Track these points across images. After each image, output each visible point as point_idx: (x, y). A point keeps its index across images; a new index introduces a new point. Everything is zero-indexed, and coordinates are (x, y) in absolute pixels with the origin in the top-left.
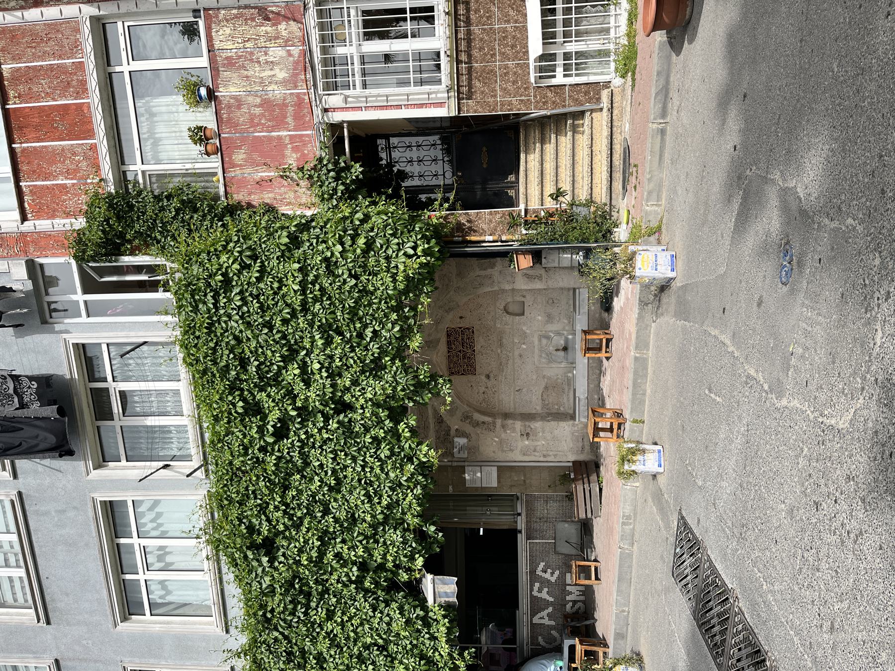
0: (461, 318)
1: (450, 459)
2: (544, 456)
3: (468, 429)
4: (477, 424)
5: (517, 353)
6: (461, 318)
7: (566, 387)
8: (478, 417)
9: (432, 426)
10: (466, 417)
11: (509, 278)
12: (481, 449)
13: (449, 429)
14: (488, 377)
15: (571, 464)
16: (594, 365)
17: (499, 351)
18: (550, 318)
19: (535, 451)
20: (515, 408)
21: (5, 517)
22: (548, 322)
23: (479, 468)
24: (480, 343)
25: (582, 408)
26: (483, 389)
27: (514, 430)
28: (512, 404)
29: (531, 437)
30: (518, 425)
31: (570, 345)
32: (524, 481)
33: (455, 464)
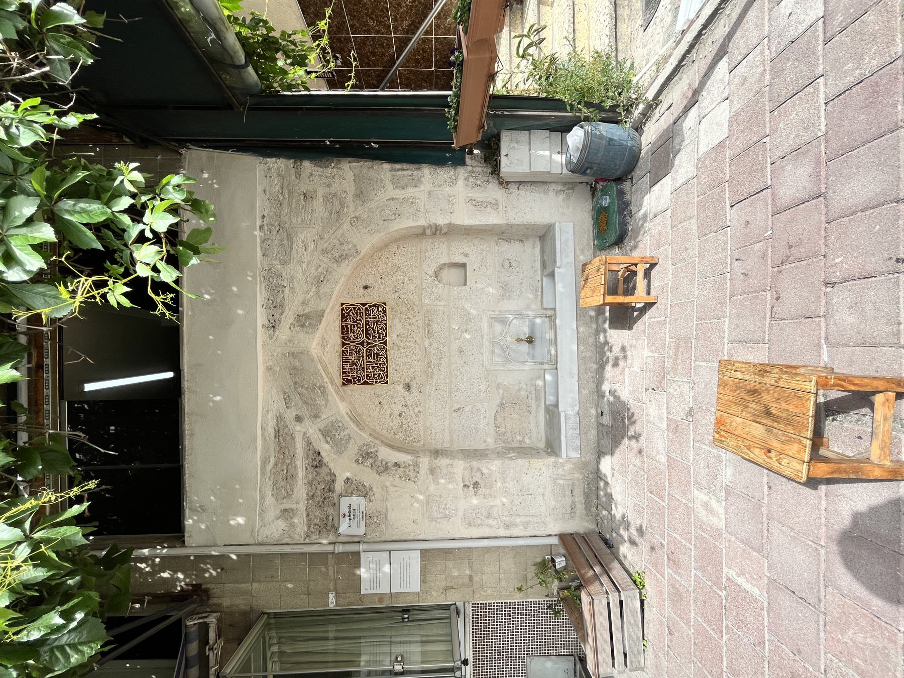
0: (366, 287)
1: (332, 538)
2: (507, 526)
3: (367, 476)
4: (384, 468)
5: (455, 346)
6: (366, 287)
7: (533, 404)
8: (386, 454)
9: (301, 473)
12: (392, 516)
14: (408, 387)
15: (555, 541)
16: (588, 354)
17: (427, 343)
18: (506, 291)
22: (502, 297)
23: (386, 555)
26: (398, 408)
27: (451, 478)
29: (482, 490)
30: (460, 467)
31: (537, 335)
32: (471, 577)
33: (340, 549)
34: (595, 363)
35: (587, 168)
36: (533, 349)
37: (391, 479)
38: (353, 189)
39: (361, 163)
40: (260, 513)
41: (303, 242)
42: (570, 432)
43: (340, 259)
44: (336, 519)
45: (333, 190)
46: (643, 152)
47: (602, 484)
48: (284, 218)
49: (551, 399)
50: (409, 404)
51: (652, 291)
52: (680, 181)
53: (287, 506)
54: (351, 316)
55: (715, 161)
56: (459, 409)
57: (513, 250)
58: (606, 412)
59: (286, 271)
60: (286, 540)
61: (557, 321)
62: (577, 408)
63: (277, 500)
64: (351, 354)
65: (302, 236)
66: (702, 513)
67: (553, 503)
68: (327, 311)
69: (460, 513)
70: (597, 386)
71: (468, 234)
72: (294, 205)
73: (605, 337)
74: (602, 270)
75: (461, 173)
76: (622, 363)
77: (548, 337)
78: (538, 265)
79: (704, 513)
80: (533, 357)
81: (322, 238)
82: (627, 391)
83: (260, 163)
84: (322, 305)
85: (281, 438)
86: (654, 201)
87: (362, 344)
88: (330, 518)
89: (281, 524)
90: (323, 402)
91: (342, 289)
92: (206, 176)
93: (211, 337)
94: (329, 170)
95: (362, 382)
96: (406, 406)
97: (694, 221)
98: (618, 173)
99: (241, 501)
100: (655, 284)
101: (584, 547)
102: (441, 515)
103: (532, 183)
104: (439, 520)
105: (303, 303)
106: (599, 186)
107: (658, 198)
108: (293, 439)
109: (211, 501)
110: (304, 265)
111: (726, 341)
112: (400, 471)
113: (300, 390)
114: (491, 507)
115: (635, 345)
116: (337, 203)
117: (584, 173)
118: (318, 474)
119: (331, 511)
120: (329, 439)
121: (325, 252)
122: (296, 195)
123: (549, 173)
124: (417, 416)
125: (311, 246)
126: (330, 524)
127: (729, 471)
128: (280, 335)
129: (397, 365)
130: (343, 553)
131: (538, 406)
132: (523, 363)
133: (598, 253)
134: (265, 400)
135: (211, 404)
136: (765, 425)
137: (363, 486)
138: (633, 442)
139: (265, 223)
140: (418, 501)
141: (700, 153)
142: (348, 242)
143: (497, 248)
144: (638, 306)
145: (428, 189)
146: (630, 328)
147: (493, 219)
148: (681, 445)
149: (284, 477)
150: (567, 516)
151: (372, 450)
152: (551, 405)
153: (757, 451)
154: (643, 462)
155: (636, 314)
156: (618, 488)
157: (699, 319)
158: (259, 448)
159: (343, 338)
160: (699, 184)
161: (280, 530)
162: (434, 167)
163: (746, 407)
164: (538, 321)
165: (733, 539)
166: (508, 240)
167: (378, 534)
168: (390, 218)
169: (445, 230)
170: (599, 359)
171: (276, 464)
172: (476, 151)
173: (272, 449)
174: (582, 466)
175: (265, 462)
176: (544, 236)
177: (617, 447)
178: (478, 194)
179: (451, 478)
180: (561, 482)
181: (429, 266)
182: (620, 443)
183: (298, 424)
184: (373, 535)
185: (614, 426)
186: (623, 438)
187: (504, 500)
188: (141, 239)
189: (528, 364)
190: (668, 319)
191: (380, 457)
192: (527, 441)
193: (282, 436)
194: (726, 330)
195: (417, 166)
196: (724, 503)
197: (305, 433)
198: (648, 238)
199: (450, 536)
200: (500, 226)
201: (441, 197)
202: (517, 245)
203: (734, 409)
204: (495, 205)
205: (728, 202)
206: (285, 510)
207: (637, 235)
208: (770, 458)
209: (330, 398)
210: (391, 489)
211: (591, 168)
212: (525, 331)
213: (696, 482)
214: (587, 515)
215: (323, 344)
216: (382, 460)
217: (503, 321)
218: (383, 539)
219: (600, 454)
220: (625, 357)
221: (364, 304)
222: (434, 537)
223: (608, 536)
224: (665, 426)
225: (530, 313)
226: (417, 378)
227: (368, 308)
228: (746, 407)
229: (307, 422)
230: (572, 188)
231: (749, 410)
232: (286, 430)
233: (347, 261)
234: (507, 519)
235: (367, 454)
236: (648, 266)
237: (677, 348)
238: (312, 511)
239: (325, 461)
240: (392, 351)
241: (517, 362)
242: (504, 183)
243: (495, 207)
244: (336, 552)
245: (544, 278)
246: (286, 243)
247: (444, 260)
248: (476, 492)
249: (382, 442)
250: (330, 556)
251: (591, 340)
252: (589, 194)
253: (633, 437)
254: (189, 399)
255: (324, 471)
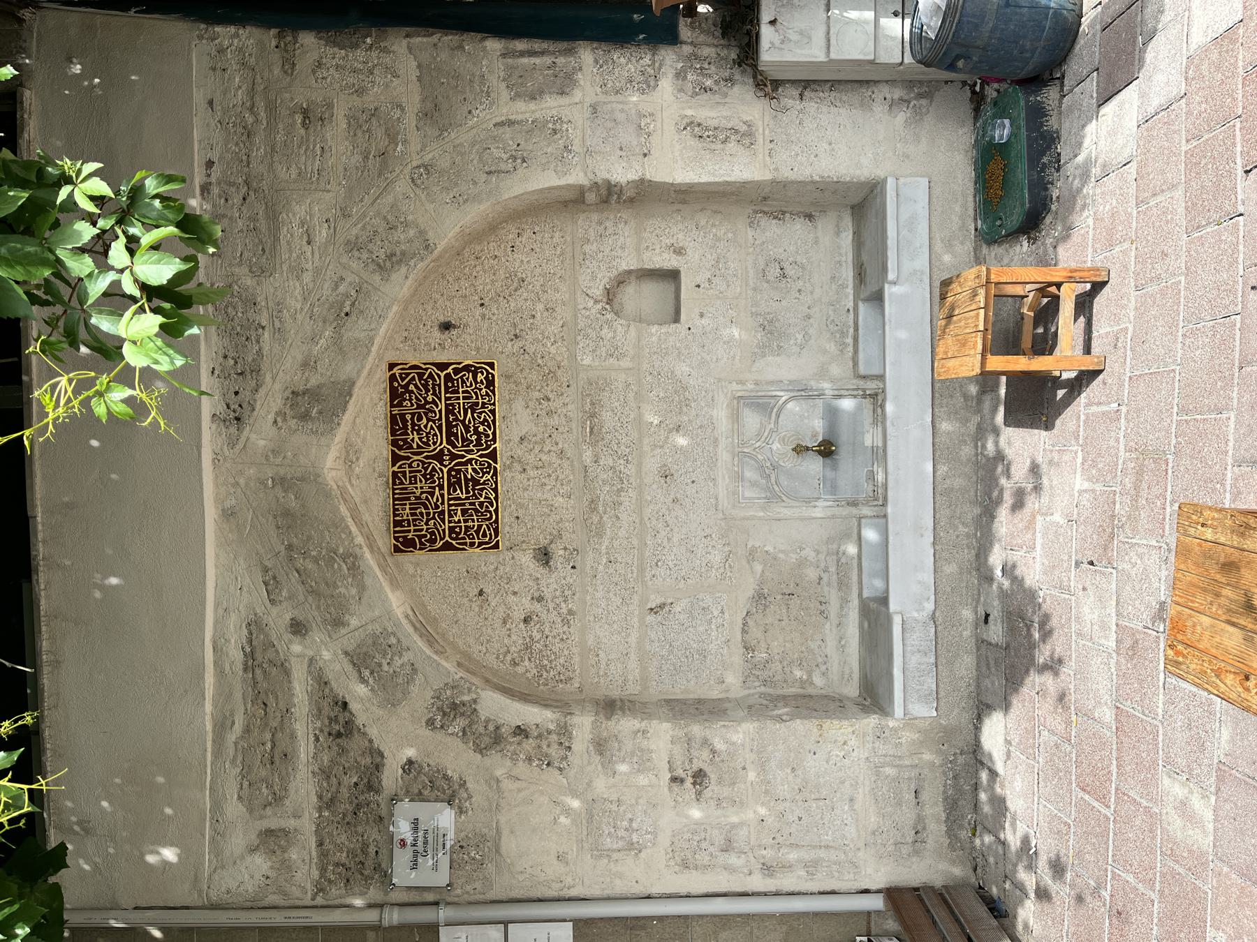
0: (446, 326)
1: (375, 894)
2: (768, 869)
3: (455, 757)
4: (492, 739)
5: (652, 464)
6: (446, 326)
7: (833, 597)
8: (498, 708)
9: (304, 750)
10: (451, 711)
11: (627, 136)
12: (509, 845)
13: (377, 759)
14: (544, 556)
16: (958, 482)
17: (588, 456)
18: (771, 333)
19: (728, 847)
20: (644, 680)
21: (670, 897)
22: (763, 350)
24: (514, 423)
25: (914, 660)
27: (643, 762)
28: (633, 664)
29: (713, 790)
30: (662, 737)
31: (844, 437)
33: (394, 917)
34: (975, 503)
35: (958, 57)
36: (835, 468)
37: (508, 763)
38: (417, 98)
39: (435, 38)
40: (213, 840)
41: (302, 224)
42: (914, 660)
43: (390, 262)
44: (383, 857)
45: (369, 100)
46: (1084, 27)
47: (984, 776)
48: (258, 167)
49: (873, 586)
50: (548, 594)
51: (1094, 344)
52: (1156, 102)
53: (274, 824)
54: (404, 386)
55: (1218, 68)
56: (662, 606)
57: (789, 238)
58: (995, 614)
59: (266, 290)
60: (273, 899)
61: (889, 408)
62: (930, 606)
63: (251, 810)
64: (413, 480)
65: (300, 210)
66: (1175, 823)
67: (873, 819)
68: (359, 383)
69: (664, 840)
70: (978, 556)
71: (684, 202)
72: (279, 138)
73: (996, 443)
74: (981, 298)
75: (668, 62)
76: (1031, 503)
77: (868, 443)
78: (848, 274)
79: (1179, 822)
80: (834, 489)
81: (346, 215)
82: (1038, 566)
83: (200, 37)
84: (349, 369)
85: (258, 671)
86: (1107, 136)
87: (439, 457)
88: (372, 850)
89: (260, 864)
90: (354, 591)
91: (393, 331)
92: (77, 69)
93: (95, 443)
94: (360, 54)
95: (439, 544)
96: (540, 599)
97: (1179, 193)
98: (1030, 67)
99: (168, 811)
100: (1101, 329)
101: (940, 914)
102: (621, 844)
103: (834, 84)
104: (615, 856)
105: (305, 365)
106: (991, 92)
107: (1113, 133)
108: (287, 673)
109: (102, 810)
110: (307, 278)
111: (1230, 461)
112: (529, 745)
113: (300, 562)
114: (734, 826)
115: (1056, 464)
116: (379, 133)
117: (951, 67)
118: (343, 751)
119: (373, 834)
120: (367, 673)
121: (353, 246)
122: (285, 112)
123: (872, 62)
124: (566, 622)
125: (322, 234)
126: (369, 863)
127: (1225, 734)
128: (253, 437)
129: (521, 506)
130: (401, 927)
131: (844, 601)
132: (808, 501)
133: (985, 250)
134: (221, 587)
135: (98, 595)
136: (1243, 628)
137: (446, 777)
138: (1047, 679)
139: (213, 179)
140: (568, 811)
141: (1193, 46)
142: (406, 225)
143: (750, 233)
144: (1065, 376)
145: (590, 99)
146: (1048, 426)
147: (739, 167)
148: (1141, 682)
149: (266, 761)
150: (905, 850)
151: (466, 698)
152: (875, 599)
153: (1230, 679)
154: (1068, 723)
155: (1061, 393)
156: (1018, 784)
157: (1183, 410)
158: (209, 694)
159: (394, 443)
160: (1189, 113)
161: (258, 876)
162: (604, 46)
163: (1218, 595)
164: (847, 404)
165: (1225, 869)
166: (779, 215)
167: (478, 885)
168: (503, 166)
169: (629, 193)
170: (980, 493)
171: (247, 730)
172: (702, 9)
173: (238, 695)
174: (941, 736)
175: (222, 726)
176: (862, 205)
177: (1016, 690)
178: (708, 112)
179: (643, 762)
180: (889, 771)
181: (594, 278)
182: (1021, 683)
183: (297, 639)
184: (468, 888)
185: (1007, 646)
186: (1027, 672)
187: (762, 811)
188: (115, 300)
189: (820, 503)
190: (1124, 409)
191: (483, 713)
192: (818, 680)
193: (261, 665)
194: (1231, 438)
195: (564, 45)
196: (1213, 798)
197: (312, 661)
198: (1090, 221)
199: (639, 890)
200: (758, 185)
201: (621, 117)
202: (799, 227)
203: (1200, 600)
204: (746, 136)
205: (1239, 161)
206: (269, 833)
207: (1070, 209)
208: (1247, 690)
209: (368, 581)
210: (507, 785)
211: (967, 58)
212: (816, 427)
213: (1167, 762)
214: (951, 846)
215: (350, 456)
216: (488, 721)
217: (764, 405)
218: (491, 895)
219: (981, 710)
220: (1037, 489)
221: (442, 366)
222: (607, 892)
223: (994, 891)
224: (1112, 644)
225: (826, 385)
226: (566, 535)
227: (454, 376)
228: (1218, 595)
229: (317, 636)
230: (928, 95)
231: (1222, 601)
232: (270, 654)
233: (404, 270)
234: (768, 853)
235: (454, 706)
236: (1088, 286)
237: (1140, 473)
238: (330, 834)
239: (359, 721)
240: (508, 474)
241: (796, 499)
242: (769, 86)
243: (747, 141)
244: (386, 923)
245: (861, 306)
246: (263, 225)
247: (628, 262)
248: (699, 794)
249: (487, 681)
250: (371, 935)
251: (967, 451)
252: (967, 108)
253: (1045, 668)
254: (48, 583)
255: (355, 745)
